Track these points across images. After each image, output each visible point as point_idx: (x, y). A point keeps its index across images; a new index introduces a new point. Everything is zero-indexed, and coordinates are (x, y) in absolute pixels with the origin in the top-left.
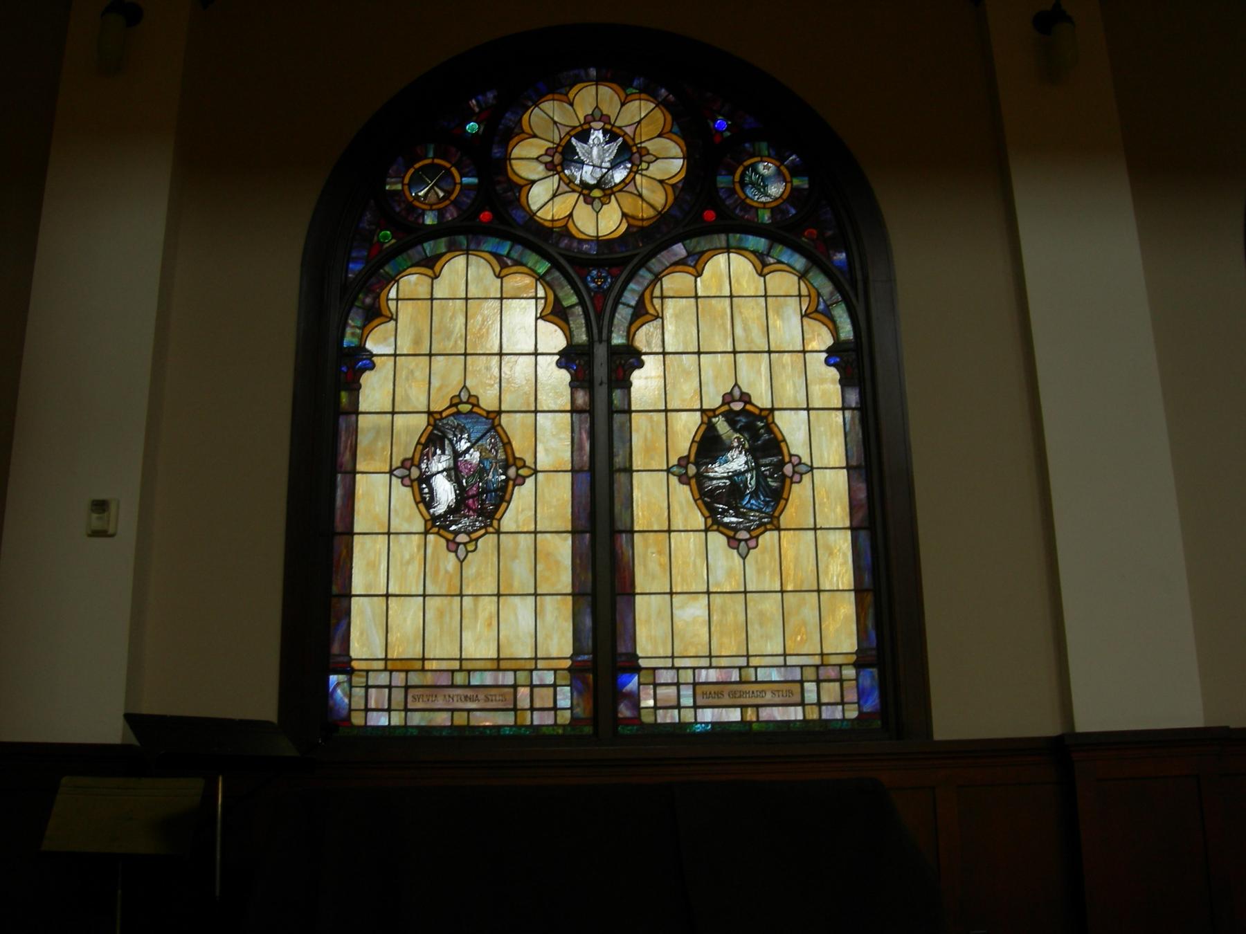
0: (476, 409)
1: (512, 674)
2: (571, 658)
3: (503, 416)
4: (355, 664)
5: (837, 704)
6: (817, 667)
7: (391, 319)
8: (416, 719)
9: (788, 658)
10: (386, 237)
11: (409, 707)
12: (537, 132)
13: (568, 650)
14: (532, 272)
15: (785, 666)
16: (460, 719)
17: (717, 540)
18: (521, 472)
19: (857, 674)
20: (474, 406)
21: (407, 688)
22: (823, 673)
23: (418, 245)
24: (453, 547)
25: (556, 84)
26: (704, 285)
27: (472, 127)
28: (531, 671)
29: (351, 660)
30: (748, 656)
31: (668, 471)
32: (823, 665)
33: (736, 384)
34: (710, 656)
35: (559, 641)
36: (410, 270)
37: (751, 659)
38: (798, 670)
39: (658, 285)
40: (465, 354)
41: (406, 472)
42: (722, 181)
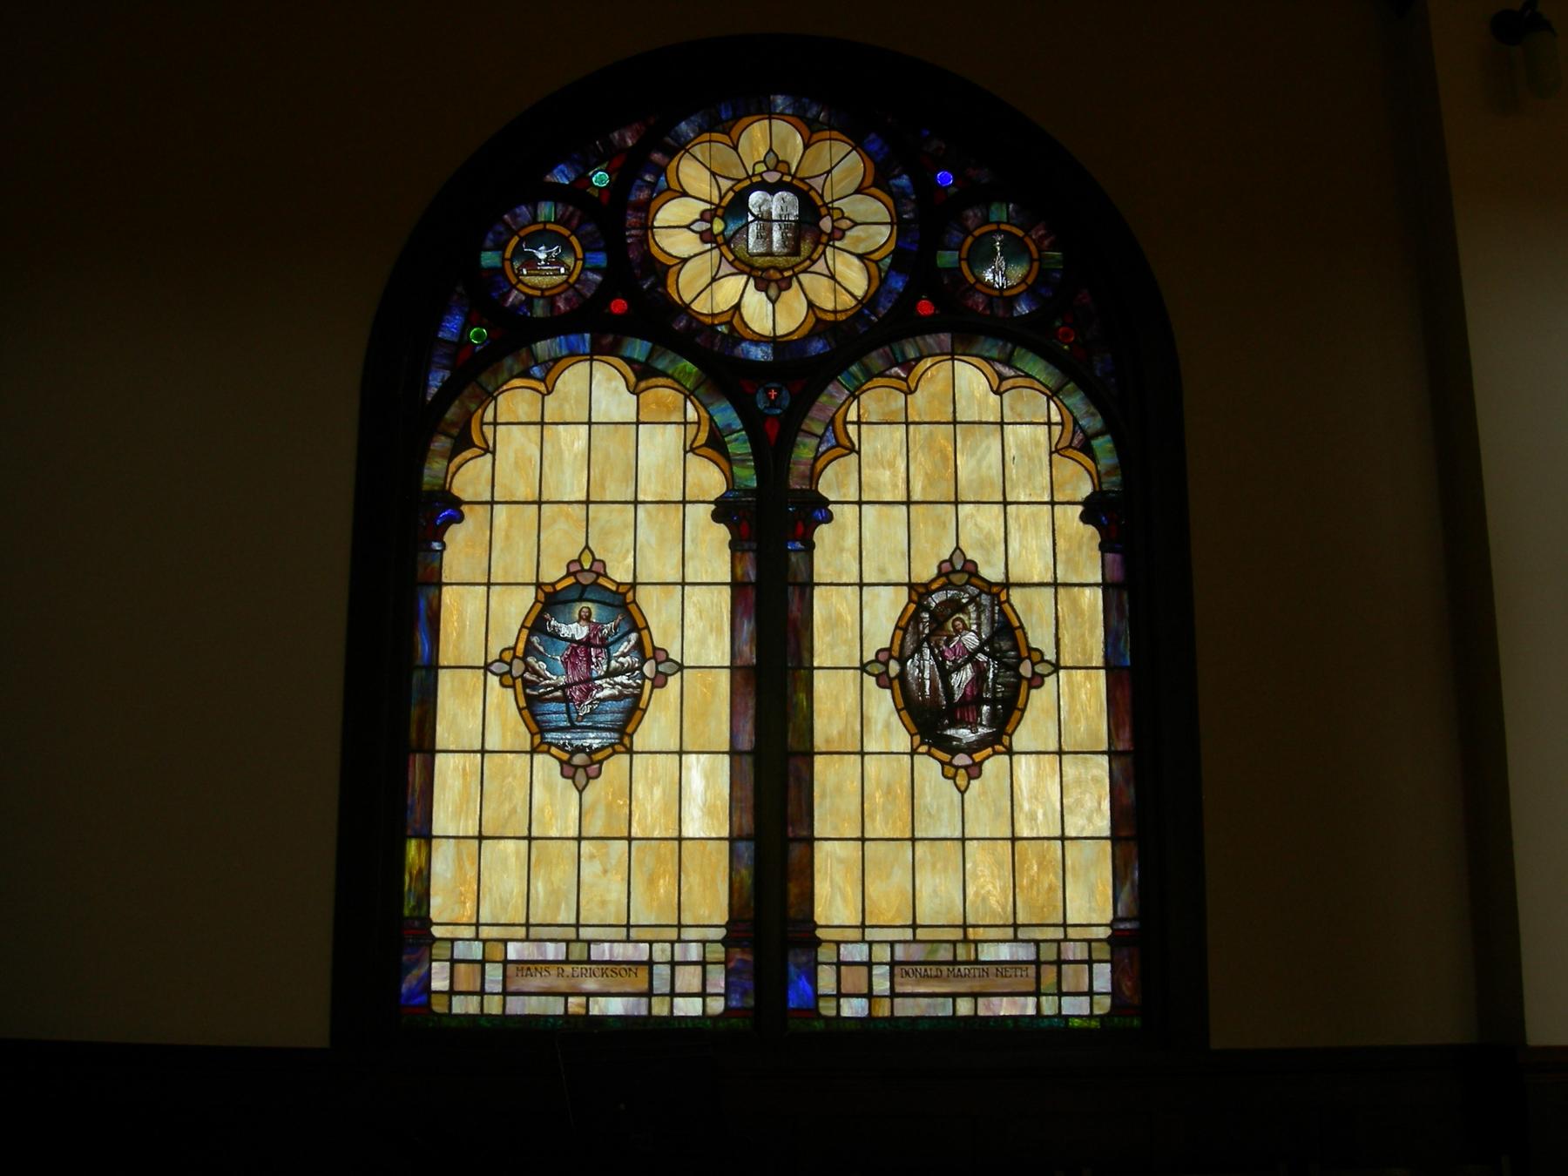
1: (949, 947)
2: (1110, 925)
4: (820, 933)
5: (1088, 995)
7: (486, 451)
9: (532, 930)
10: (478, 336)
14: (678, 384)
16: (575, 1004)
18: (1039, 669)
19: (727, 953)
23: (521, 341)
25: (725, 109)
26: (920, 402)
28: (672, 943)
29: (816, 926)
31: (863, 668)
35: (710, 903)
39: (492, 406)
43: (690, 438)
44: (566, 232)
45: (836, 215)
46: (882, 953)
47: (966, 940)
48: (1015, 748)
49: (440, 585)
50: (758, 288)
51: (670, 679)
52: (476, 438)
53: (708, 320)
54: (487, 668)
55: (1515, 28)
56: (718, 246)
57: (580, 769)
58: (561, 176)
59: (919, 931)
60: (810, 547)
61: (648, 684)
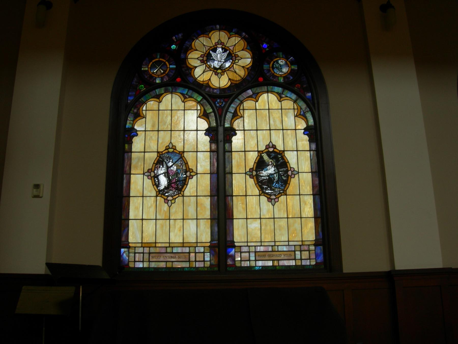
0: (175, 151)
1: (188, 248)
2: (210, 242)
3: (185, 153)
4: (130, 245)
5: (308, 259)
6: (300, 246)
7: (144, 117)
8: (153, 265)
9: (290, 242)
10: (142, 87)
11: (150, 260)
12: (197, 49)
13: (209, 240)
14: (196, 100)
15: (289, 245)
16: (169, 265)
17: (264, 199)
18: (192, 174)
19: (315, 248)
20: (174, 149)
21: (150, 253)
22: (303, 248)
23: (154, 90)
24: (166, 201)
25: (205, 31)
26: (259, 105)
27: (173, 47)
28: (195, 247)
29: (129, 243)
30: (275, 242)
31: (246, 173)
32: (302, 245)
33: (271, 142)
34: (261, 242)
35: (206, 236)
36: (151, 100)
37: (276, 243)
38: (293, 247)
39: (242, 105)
40: (171, 131)
41: (149, 174)
42: (266, 67)
46: (147, 250)
55: (385, 8)
56: (205, 64)
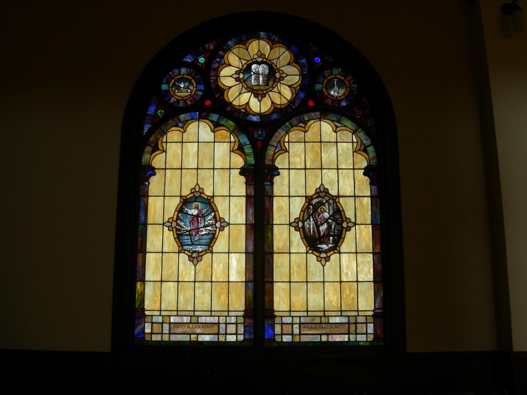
1: (319, 318)
2: (373, 311)
4: (276, 313)
5: (366, 334)
7: (163, 151)
9: (179, 312)
10: (161, 113)
14: (228, 129)
16: (193, 337)
18: (349, 225)
19: (244, 320)
23: (175, 115)
25: (244, 37)
26: (309, 135)
28: (226, 317)
29: (274, 311)
31: (290, 224)
35: (238, 303)
39: (165, 136)
43: (232, 147)
44: (190, 78)
45: (281, 72)
46: (297, 320)
47: (325, 316)
48: (341, 251)
49: (148, 196)
50: (255, 97)
51: (225, 228)
52: (160, 147)
53: (238, 108)
54: (164, 224)
55: (509, 9)
57: (195, 258)
58: (189, 59)
59: (309, 313)
60: (272, 184)
61: (218, 230)
